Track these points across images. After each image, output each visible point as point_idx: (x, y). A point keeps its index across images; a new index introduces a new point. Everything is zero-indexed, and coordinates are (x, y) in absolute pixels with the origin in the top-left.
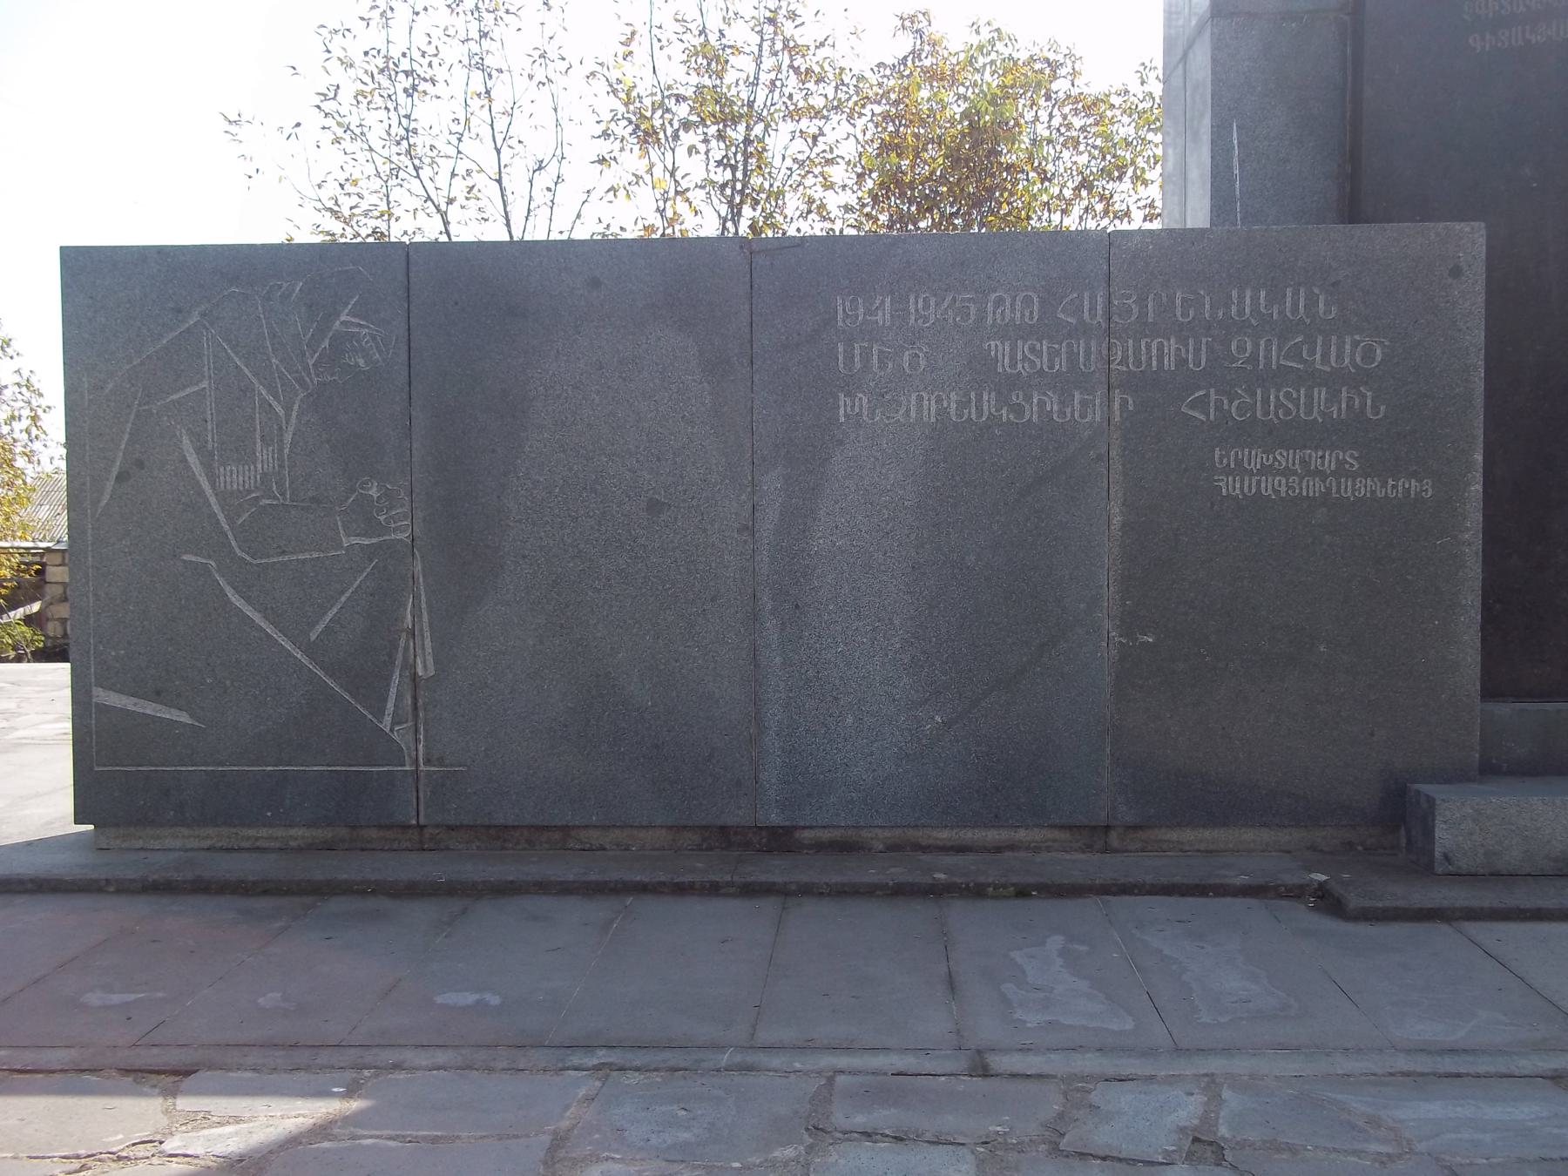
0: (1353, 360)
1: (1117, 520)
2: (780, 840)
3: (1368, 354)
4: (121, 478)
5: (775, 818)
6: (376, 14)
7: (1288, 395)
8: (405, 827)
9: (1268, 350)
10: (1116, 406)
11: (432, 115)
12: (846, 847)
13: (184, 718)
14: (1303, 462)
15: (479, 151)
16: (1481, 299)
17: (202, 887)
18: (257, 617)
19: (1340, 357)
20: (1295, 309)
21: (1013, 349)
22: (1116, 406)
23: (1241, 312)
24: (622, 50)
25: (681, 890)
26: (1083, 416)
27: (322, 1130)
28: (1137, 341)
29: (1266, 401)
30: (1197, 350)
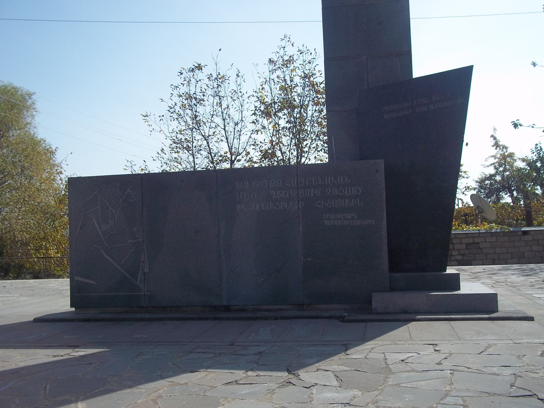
0: (354, 193)
1: (301, 232)
2: (227, 309)
3: (358, 191)
4: (81, 228)
5: (225, 303)
6: (186, 82)
7: (340, 201)
8: (142, 307)
9: (335, 191)
10: (300, 205)
11: (203, 111)
12: (243, 310)
13: (94, 283)
14: (344, 217)
15: (218, 120)
16: (384, 178)
17: (96, 320)
18: (110, 259)
19: (351, 192)
20: (340, 181)
21: (276, 193)
22: (300, 205)
23: (328, 182)
24: (261, 87)
25: (200, 319)
26: (293, 207)
27: (99, 353)
28: (304, 190)
29: (335, 203)
30: (318, 192)
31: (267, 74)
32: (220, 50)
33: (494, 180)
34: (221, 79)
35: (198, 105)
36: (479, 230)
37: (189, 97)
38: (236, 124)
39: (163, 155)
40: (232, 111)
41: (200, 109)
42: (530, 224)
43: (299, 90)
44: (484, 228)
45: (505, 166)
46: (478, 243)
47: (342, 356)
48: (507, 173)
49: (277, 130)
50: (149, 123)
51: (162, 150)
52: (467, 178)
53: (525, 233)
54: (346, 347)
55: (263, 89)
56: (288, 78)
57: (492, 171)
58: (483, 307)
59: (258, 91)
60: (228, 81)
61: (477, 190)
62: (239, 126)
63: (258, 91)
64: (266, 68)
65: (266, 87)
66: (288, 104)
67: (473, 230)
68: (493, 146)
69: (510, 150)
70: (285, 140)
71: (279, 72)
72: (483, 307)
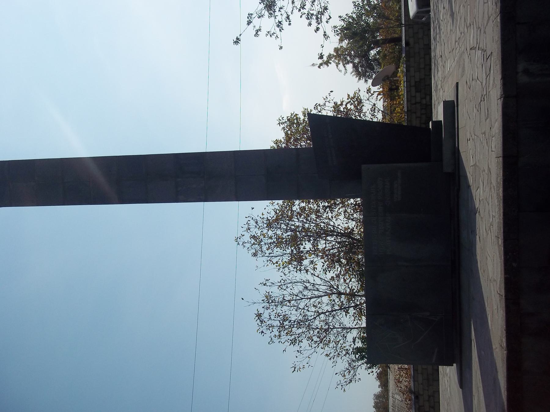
11: (294, 316)
31: (265, 259)
32: (243, 299)
33: (358, 64)
34: (268, 298)
35: (290, 319)
36: (404, 82)
37: (282, 326)
38: (306, 288)
39: (331, 355)
40: (296, 291)
41: (293, 318)
42: (399, 39)
43: (279, 232)
44: (401, 76)
45: (346, 54)
46: (416, 82)
47: (472, 188)
48: (352, 53)
49: (315, 251)
50: (302, 367)
51: (327, 355)
52: (359, 91)
53: (407, 44)
54: (469, 187)
55: (277, 263)
56: (270, 241)
57: (350, 67)
58: (451, 108)
59: (278, 267)
60: (270, 293)
61: (367, 79)
62: (308, 285)
63: (278, 267)
64: (261, 260)
65: (275, 260)
66: (294, 241)
67: (404, 86)
68: (328, 66)
69: (332, 53)
70: (322, 245)
71: (264, 248)
72: (451, 108)
